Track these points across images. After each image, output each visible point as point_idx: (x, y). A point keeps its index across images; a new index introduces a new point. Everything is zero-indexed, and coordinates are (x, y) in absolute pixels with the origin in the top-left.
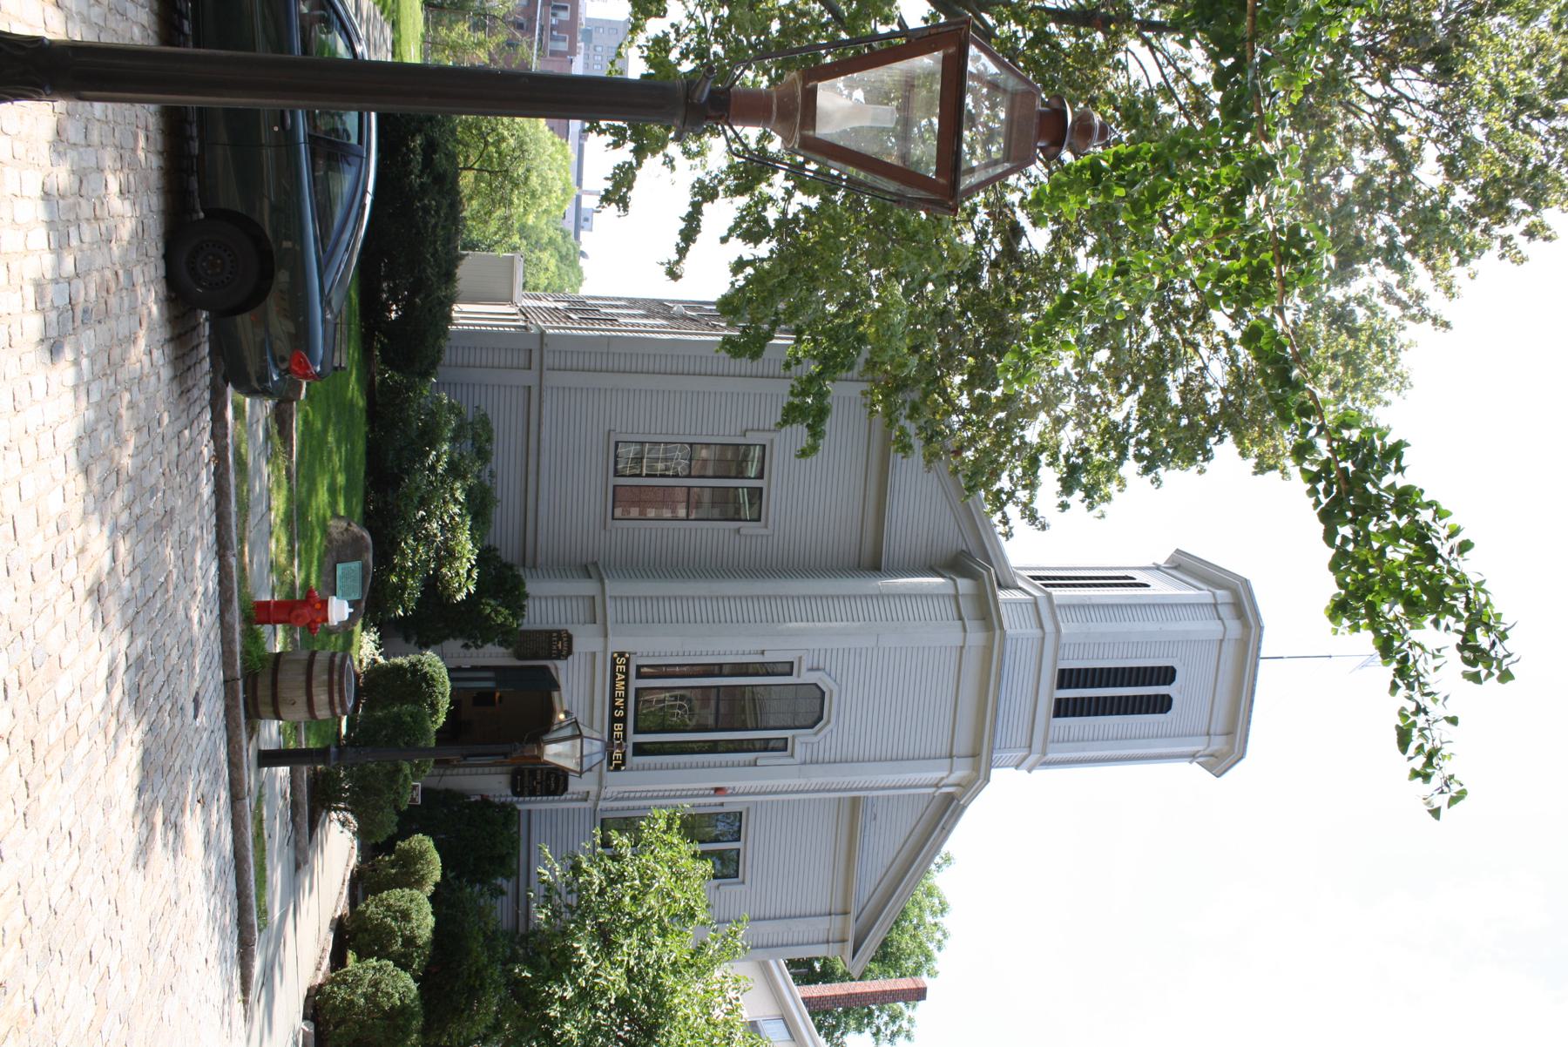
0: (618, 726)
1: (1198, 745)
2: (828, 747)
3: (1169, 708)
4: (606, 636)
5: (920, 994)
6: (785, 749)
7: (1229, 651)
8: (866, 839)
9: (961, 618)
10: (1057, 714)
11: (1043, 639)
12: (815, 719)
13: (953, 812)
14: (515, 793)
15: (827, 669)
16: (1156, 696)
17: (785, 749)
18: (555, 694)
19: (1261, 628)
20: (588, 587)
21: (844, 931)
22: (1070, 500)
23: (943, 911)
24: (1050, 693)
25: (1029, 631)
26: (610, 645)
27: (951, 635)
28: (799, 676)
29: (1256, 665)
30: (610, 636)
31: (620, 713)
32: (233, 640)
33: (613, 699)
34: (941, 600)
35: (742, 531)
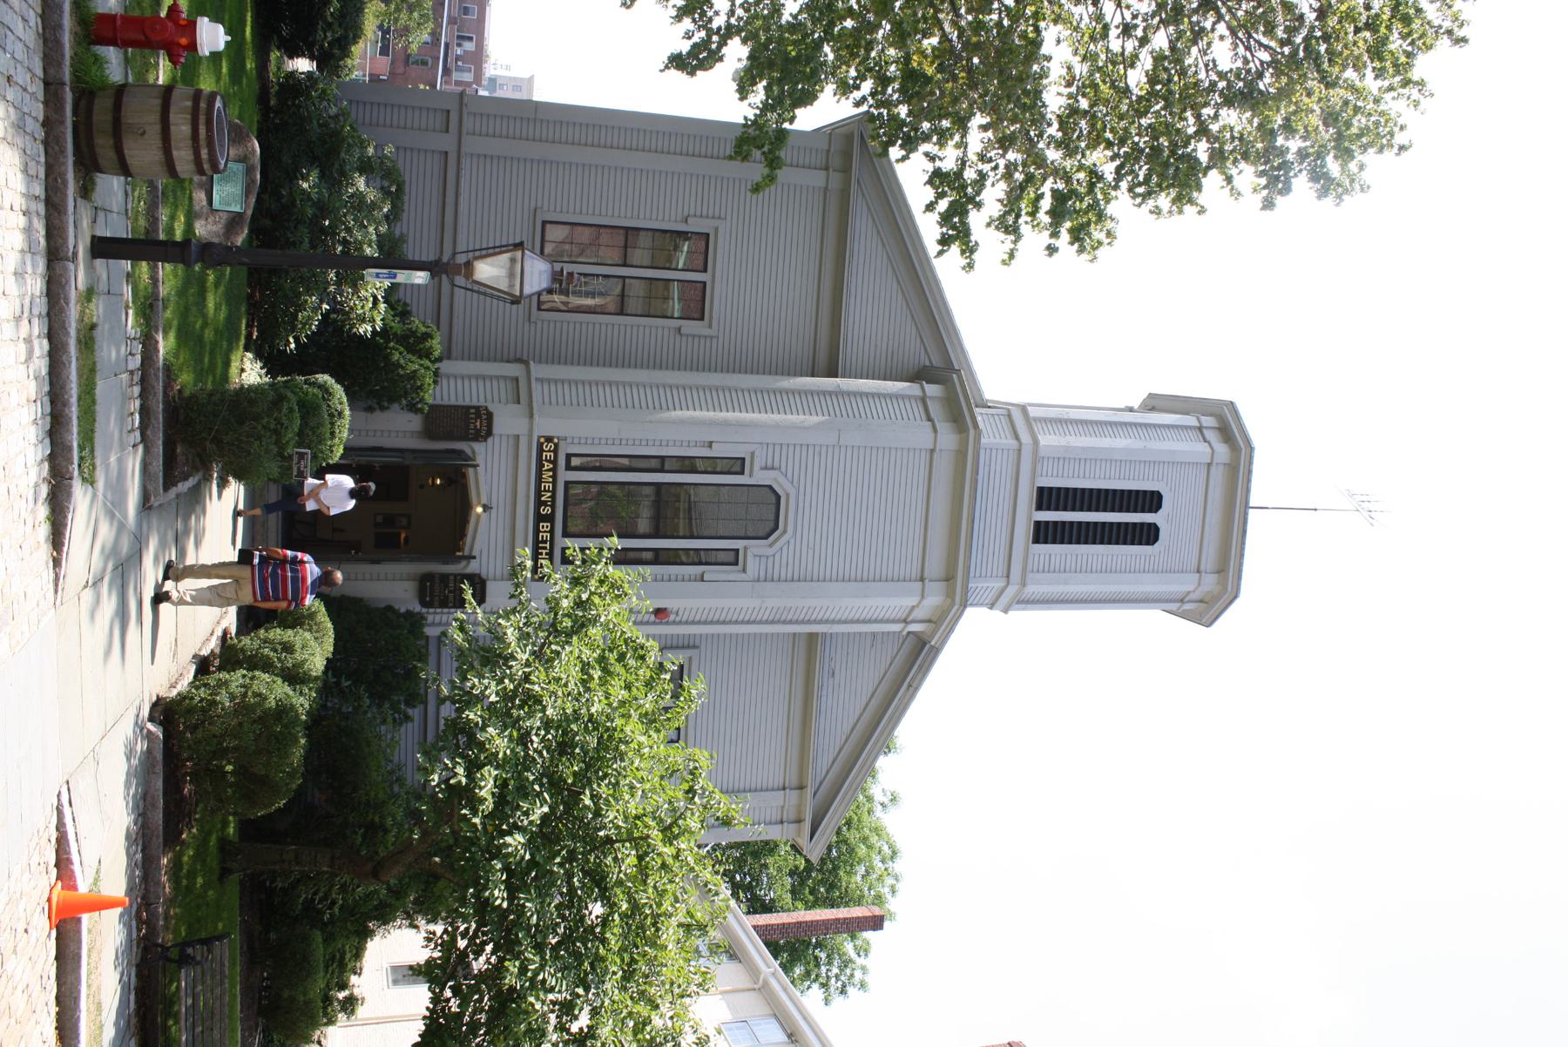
0: (545, 526)
1: (1183, 584)
3: (1156, 539)
4: (531, 416)
5: (876, 923)
6: (736, 563)
7: (1218, 475)
8: (824, 699)
9: (929, 419)
10: (1036, 540)
11: (1020, 450)
12: (770, 529)
13: (920, 667)
14: (424, 604)
15: (783, 469)
16: (1142, 524)
17: (736, 563)
19: (1251, 449)
20: (514, 370)
21: (800, 808)
23: (894, 853)
24: (1028, 515)
25: (1004, 441)
26: (535, 427)
27: (920, 435)
29: (1246, 514)
30: (536, 416)
31: (548, 510)
32: (60, 26)
33: (539, 493)
35: (683, 331)
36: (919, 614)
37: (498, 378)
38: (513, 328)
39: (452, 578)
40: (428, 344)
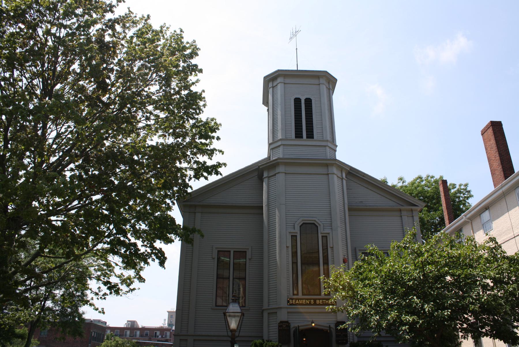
0: (318, 302)
2: (325, 220)
4: (281, 308)
5: (445, 182)
6: (326, 237)
7: (288, 80)
8: (370, 204)
10: (313, 138)
11: (284, 145)
14: (346, 343)
18: (300, 328)
20: (265, 315)
22: (216, 136)
24: (305, 141)
27: (280, 179)
28: (297, 233)
29: (300, 71)
30: (281, 306)
34: (270, 182)
35: (250, 258)
36: (339, 175)
37: (268, 320)
38: (245, 233)
39: (337, 333)
40: (258, 344)
